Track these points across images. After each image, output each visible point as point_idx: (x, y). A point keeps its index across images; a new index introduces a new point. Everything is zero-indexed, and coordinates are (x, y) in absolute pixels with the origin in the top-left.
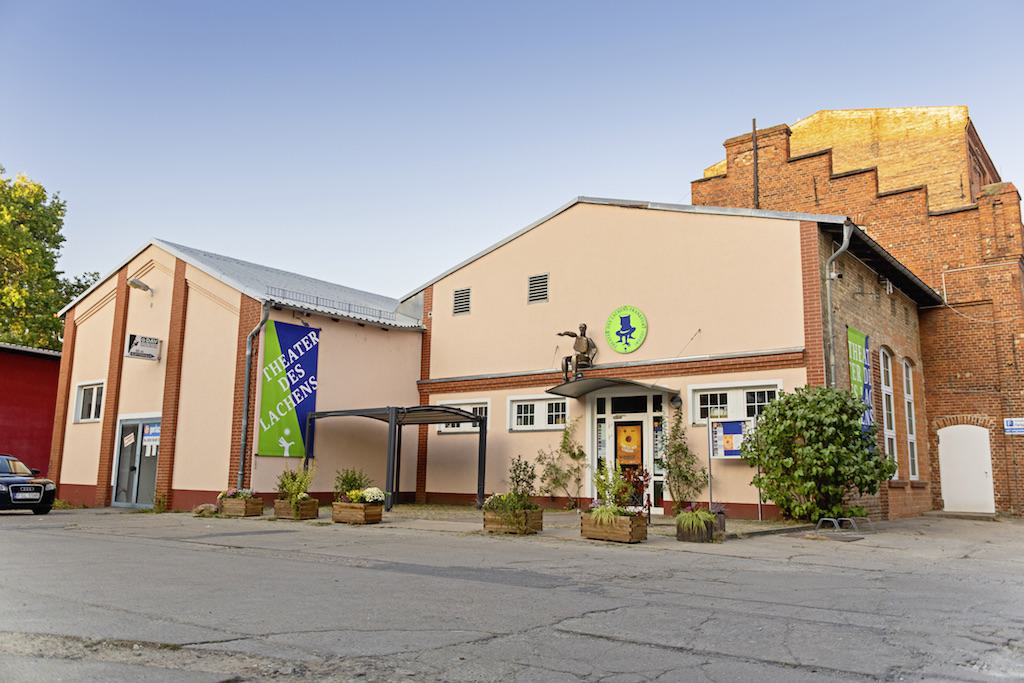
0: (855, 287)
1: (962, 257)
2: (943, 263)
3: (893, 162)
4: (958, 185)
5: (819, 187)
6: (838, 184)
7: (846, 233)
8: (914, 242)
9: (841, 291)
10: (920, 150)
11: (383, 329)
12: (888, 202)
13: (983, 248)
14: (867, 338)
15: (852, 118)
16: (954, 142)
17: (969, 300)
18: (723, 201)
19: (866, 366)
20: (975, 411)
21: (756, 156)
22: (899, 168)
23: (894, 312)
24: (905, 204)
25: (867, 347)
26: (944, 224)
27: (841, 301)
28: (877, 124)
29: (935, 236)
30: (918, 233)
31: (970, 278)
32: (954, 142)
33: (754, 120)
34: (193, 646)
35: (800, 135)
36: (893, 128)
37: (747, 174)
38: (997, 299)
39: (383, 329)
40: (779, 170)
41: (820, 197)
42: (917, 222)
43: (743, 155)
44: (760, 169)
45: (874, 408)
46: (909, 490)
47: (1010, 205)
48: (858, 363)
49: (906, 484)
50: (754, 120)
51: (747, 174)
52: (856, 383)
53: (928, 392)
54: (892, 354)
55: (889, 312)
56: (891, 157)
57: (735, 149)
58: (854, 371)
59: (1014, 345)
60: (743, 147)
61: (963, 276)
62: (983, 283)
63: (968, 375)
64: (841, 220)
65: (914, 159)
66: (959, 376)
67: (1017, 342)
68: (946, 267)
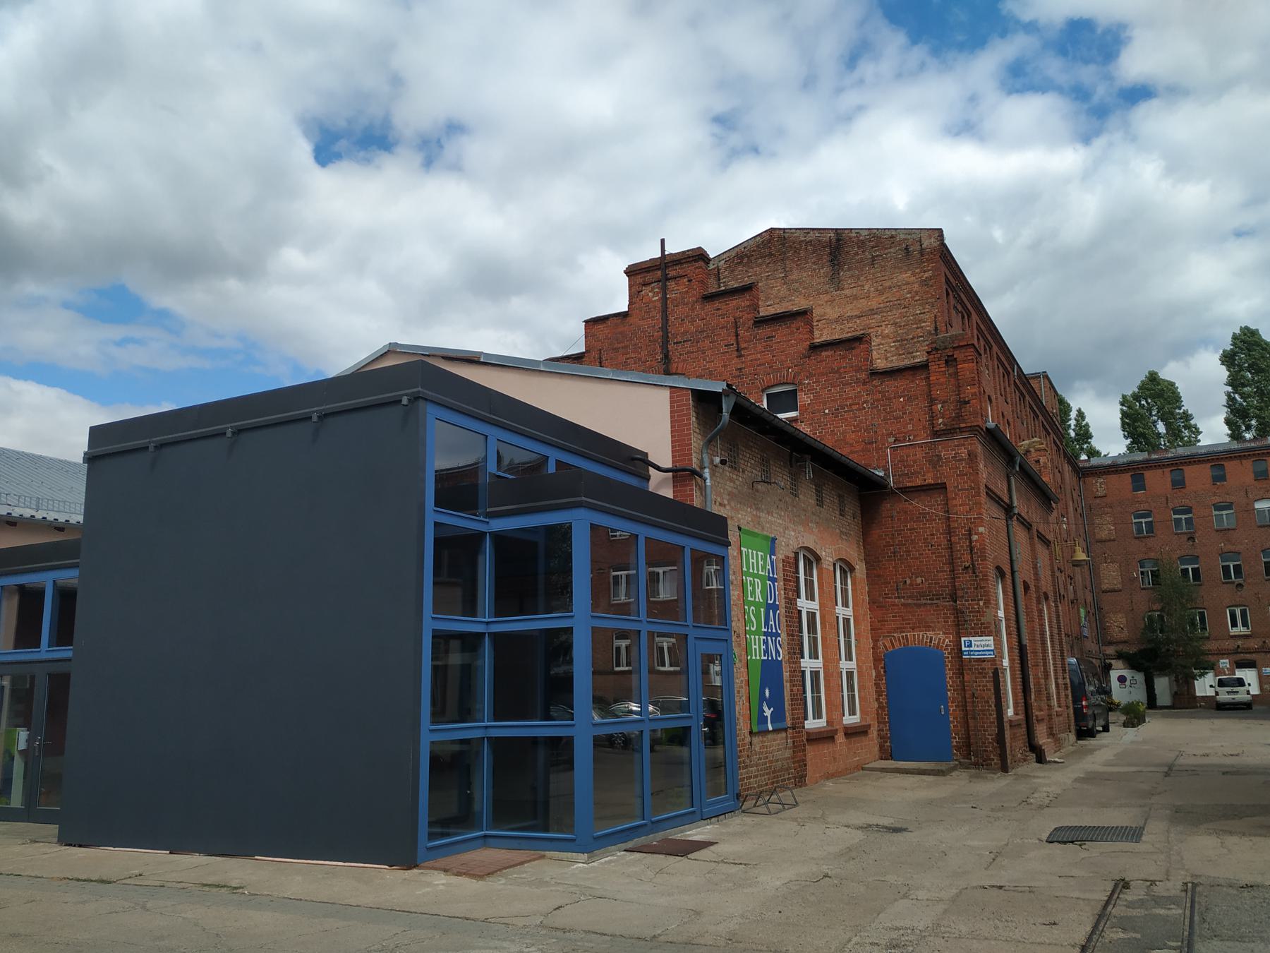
0: (756, 473)
1: (910, 427)
2: (890, 435)
3: (856, 298)
4: (931, 328)
5: (741, 332)
6: (764, 331)
7: (727, 406)
8: (854, 407)
9: (731, 480)
10: (887, 284)
11: (56, 528)
12: (824, 354)
13: (933, 418)
14: (774, 540)
15: (809, 239)
16: (926, 275)
17: (919, 482)
18: (626, 347)
19: (770, 579)
20: (928, 628)
21: (664, 290)
22: (863, 304)
23: (820, 503)
24: (844, 357)
25: (773, 552)
26: (891, 385)
27: (730, 494)
28: (838, 248)
29: (878, 400)
30: (859, 396)
31: (920, 454)
32: (926, 275)
33: (663, 241)
34: (128, 881)
35: (746, 260)
36: (857, 254)
37: (654, 313)
38: (951, 483)
39: (56, 528)
40: (693, 310)
41: (743, 346)
42: (858, 381)
43: (649, 288)
44: (670, 306)
45: (784, 635)
46: (840, 738)
47: (964, 362)
48: (758, 576)
49: (836, 731)
50: (663, 241)
51: (654, 313)
52: (753, 603)
53: (873, 602)
54: (818, 559)
55: (813, 502)
56: (855, 291)
57: (639, 279)
58: (750, 588)
59: (971, 542)
60: (649, 277)
61: (912, 451)
62: (935, 461)
63: (919, 580)
64: (718, 387)
65: (882, 294)
66: (908, 581)
67: (975, 537)
68: (892, 440)
